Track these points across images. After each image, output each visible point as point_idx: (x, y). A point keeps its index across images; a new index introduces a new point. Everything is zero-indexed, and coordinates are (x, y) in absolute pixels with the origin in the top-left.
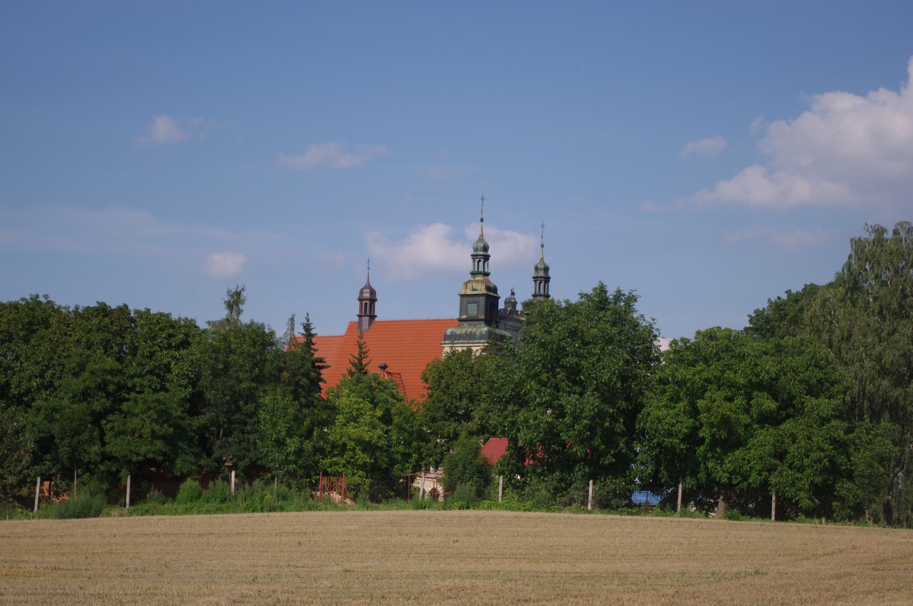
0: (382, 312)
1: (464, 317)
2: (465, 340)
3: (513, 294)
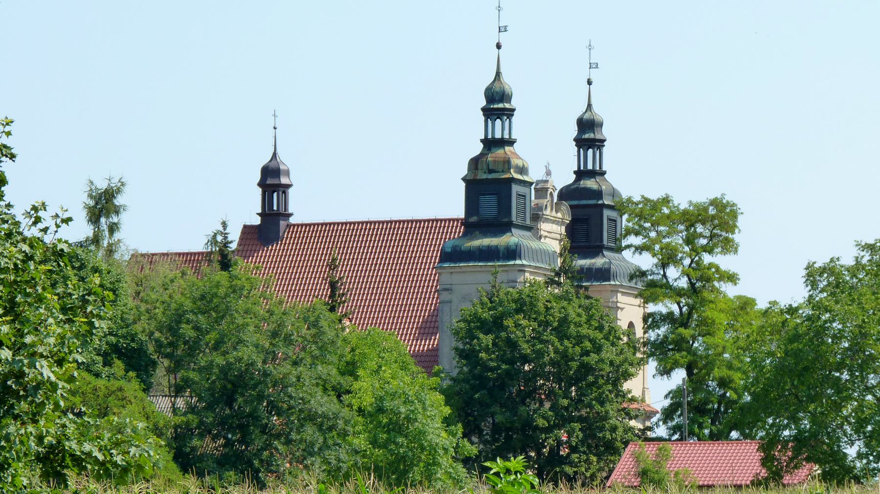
1: (474, 219)
2: (480, 261)
3: (549, 173)
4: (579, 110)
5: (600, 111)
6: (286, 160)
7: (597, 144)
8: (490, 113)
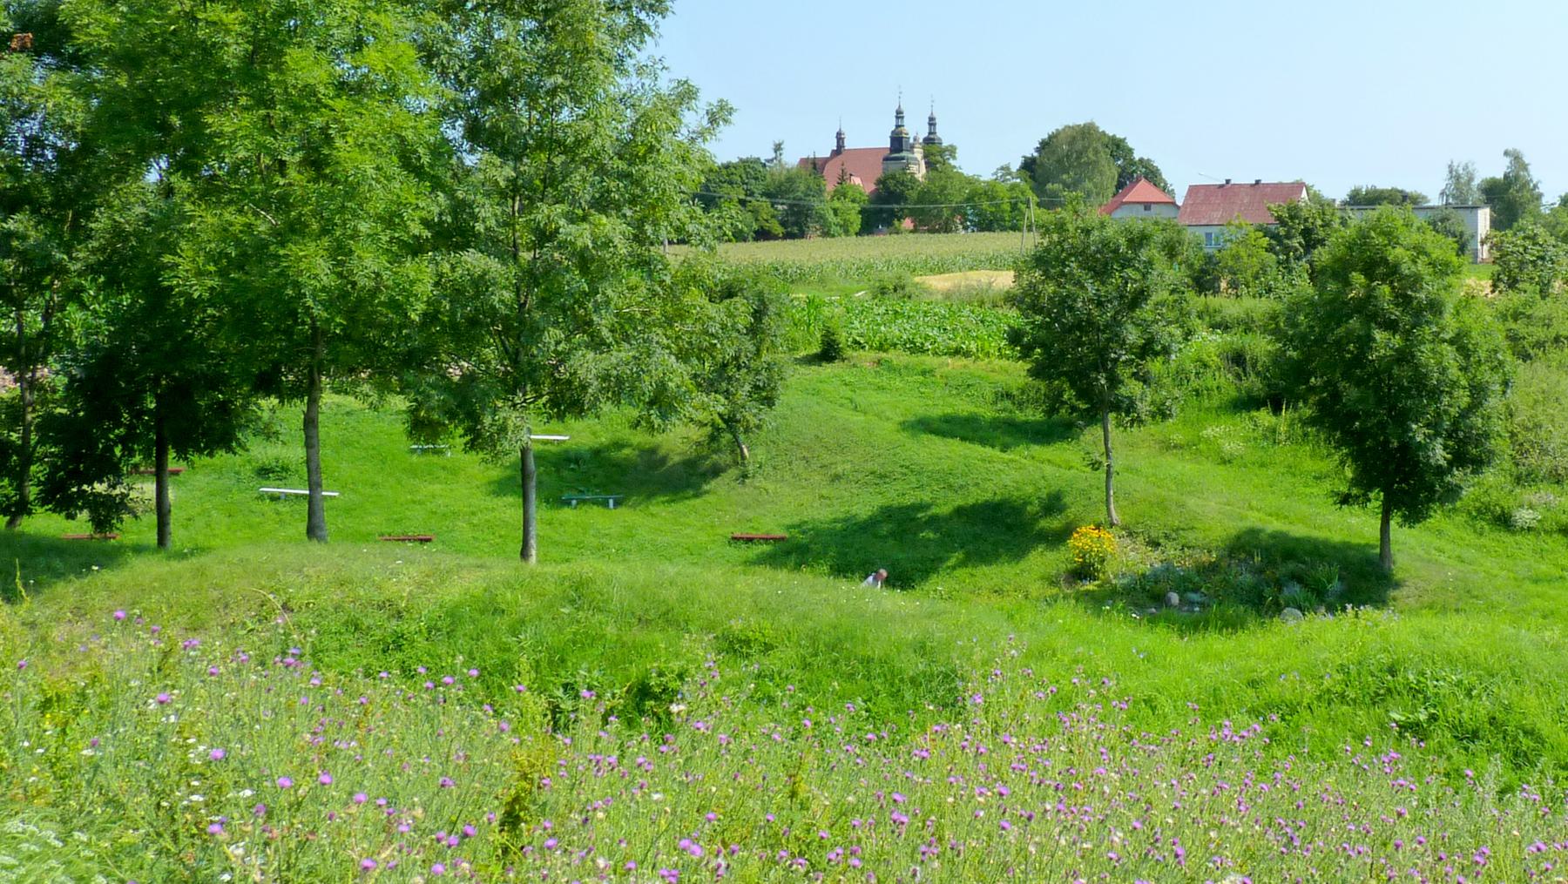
0: (849, 144)
4: (929, 115)
5: (935, 115)
6: (843, 130)
7: (934, 125)
8: (897, 118)
